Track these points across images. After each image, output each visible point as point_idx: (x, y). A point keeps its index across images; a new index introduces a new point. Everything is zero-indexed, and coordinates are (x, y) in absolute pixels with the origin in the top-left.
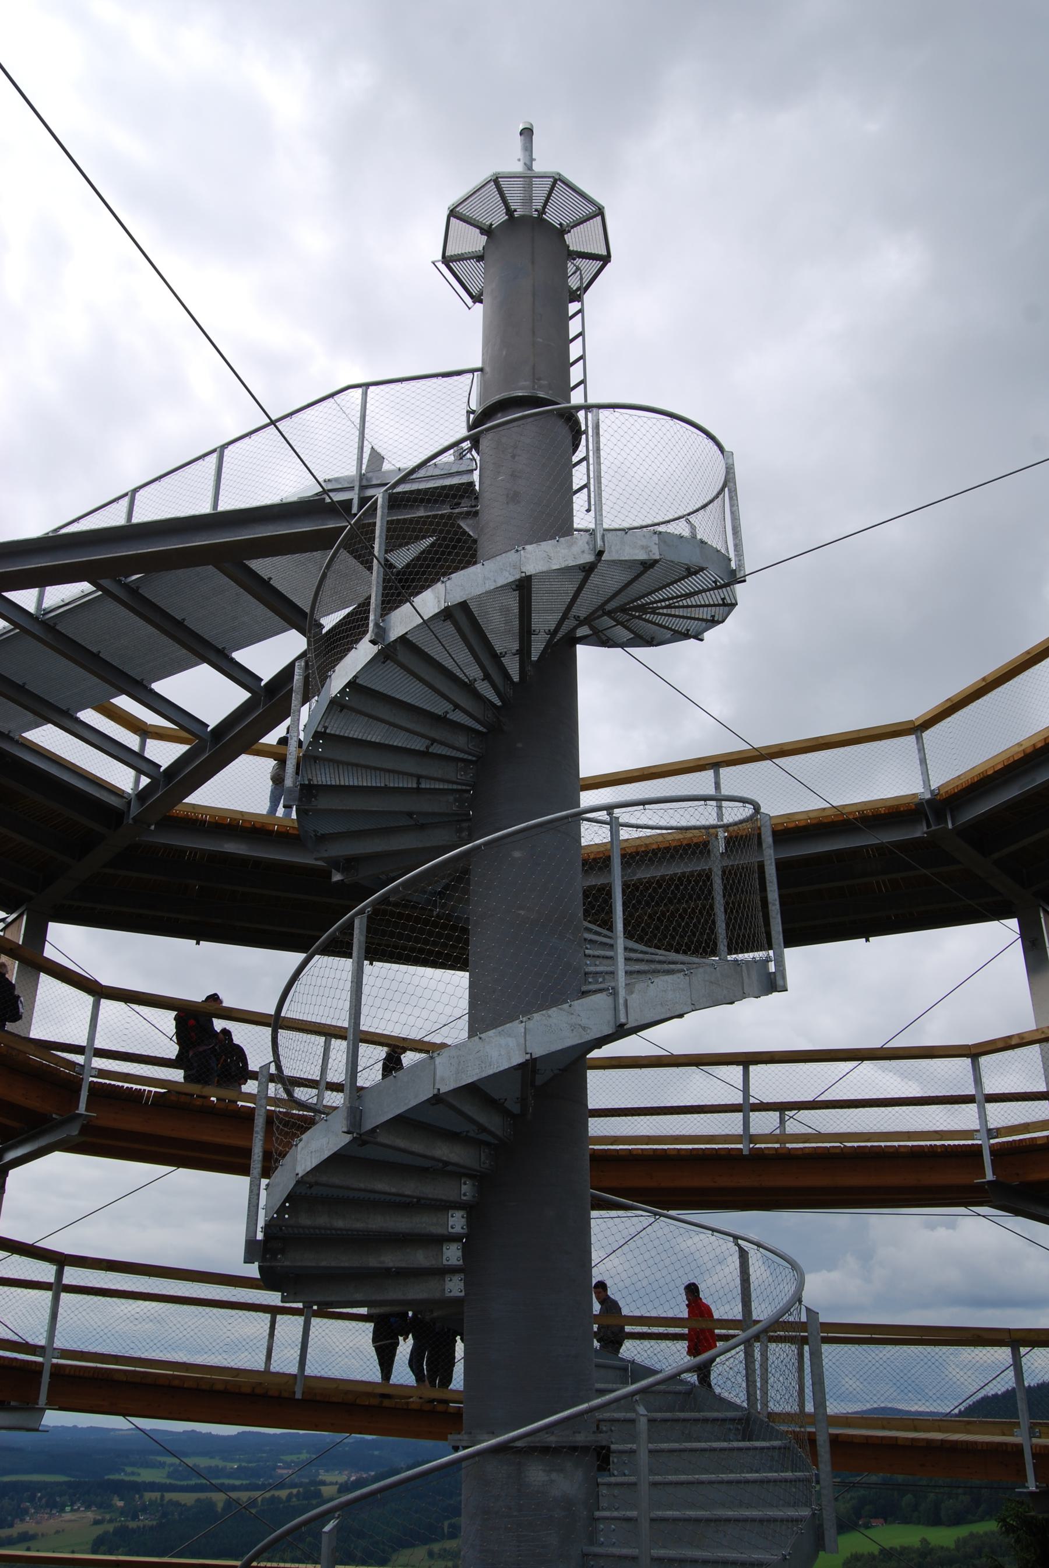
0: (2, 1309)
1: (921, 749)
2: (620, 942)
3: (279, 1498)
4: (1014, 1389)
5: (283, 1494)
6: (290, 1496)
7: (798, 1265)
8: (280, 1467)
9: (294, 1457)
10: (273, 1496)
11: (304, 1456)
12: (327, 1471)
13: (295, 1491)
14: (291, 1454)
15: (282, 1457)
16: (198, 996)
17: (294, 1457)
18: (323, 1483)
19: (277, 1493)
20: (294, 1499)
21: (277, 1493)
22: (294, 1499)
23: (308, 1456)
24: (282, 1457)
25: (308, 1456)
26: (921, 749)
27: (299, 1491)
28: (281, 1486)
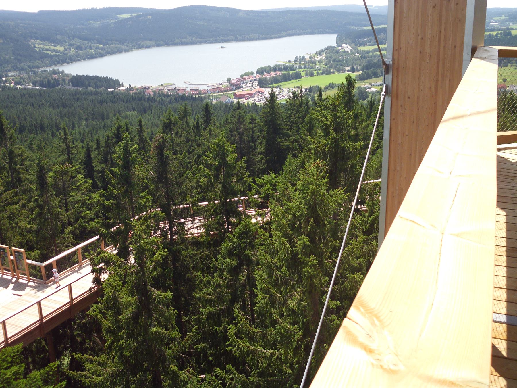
0: (516, 108)
1: (348, 318)
2: (312, 146)
3: (493, 35)
4: (127, 260)
5: (494, 33)
6: (497, 34)
7: (247, 73)
8: (492, 22)
9: (498, 18)
10: (490, 35)
11: (503, 17)
12: (513, 24)
13: (499, 32)
14: (497, 17)
15: (493, 18)
16: (88, 289)
17: (498, 18)
18: (512, 29)
19: (491, 33)
20: (499, 36)
21: (491, 33)
22: (499, 36)
23: (505, 17)
24: (493, 18)
25: (505, 17)
26: (348, 318)
27: (501, 33)
28: (493, 30)
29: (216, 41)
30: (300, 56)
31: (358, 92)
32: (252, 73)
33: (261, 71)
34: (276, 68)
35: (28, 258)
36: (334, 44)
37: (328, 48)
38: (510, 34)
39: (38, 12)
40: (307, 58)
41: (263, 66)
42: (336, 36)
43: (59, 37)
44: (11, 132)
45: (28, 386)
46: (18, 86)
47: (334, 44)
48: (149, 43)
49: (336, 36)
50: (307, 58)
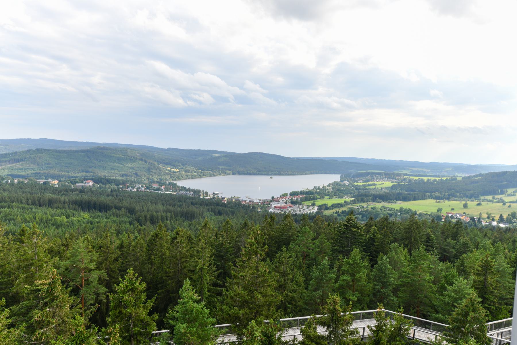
3: (443, 180)
6: (447, 179)
13: (448, 178)
19: (443, 178)
29: (268, 174)
30: (317, 186)
31: (381, 303)
32: (287, 195)
33: (293, 194)
34: (302, 193)
35: (281, 318)
36: (338, 180)
37: (334, 182)
38: (456, 179)
39: (230, 201)
40: (321, 187)
41: (294, 191)
42: (340, 175)
43: (177, 164)
44: (268, 276)
45: (339, 344)
46: (148, 190)
47: (338, 180)
48: (228, 172)
49: (340, 175)
50: (321, 187)
